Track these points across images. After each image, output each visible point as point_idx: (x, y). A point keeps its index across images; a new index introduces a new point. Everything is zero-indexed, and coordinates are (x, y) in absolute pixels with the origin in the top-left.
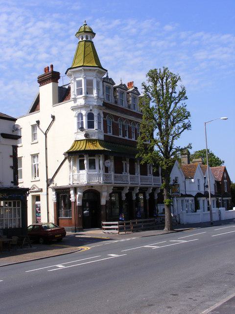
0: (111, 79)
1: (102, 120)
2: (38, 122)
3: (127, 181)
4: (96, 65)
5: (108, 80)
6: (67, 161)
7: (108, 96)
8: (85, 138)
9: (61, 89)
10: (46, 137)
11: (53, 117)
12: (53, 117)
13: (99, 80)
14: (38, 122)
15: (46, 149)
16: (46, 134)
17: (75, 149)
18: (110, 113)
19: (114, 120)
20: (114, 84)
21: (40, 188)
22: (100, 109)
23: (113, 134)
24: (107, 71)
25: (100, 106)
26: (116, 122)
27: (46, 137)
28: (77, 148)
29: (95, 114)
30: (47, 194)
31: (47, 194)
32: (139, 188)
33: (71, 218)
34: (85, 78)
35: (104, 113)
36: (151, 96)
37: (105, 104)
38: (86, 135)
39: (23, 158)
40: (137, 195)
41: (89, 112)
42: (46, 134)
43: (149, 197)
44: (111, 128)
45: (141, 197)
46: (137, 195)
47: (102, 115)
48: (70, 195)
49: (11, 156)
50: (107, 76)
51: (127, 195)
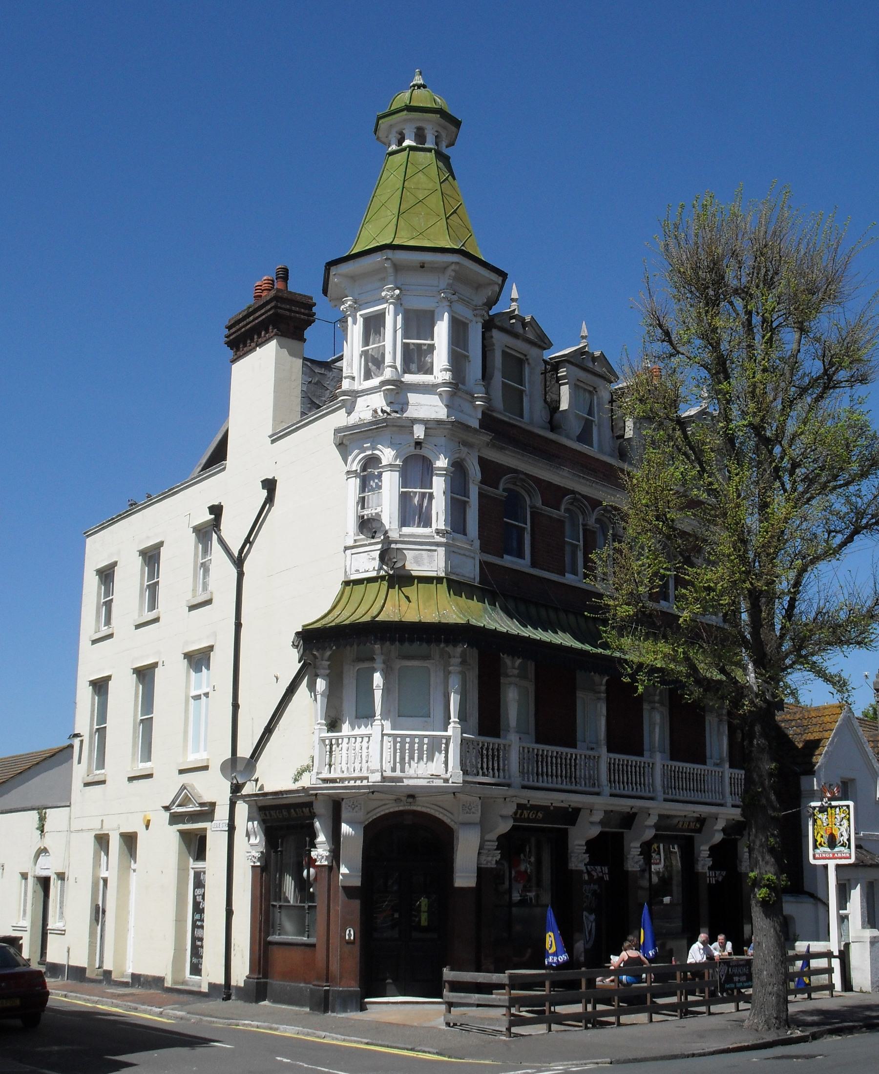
1: (474, 491)
2: (216, 511)
3: (594, 781)
6: (221, 980)
7: (514, 398)
11: (270, 485)
12: (270, 485)
13: (466, 313)
14: (216, 511)
15: (238, 626)
16: (239, 562)
17: (345, 616)
19: (539, 503)
20: (543, 343)
21: (207, 799)
22: (465, 444)
23: (534, 565)
25: (467, 428)
26: (554, 513)
27: (241, 575)
28: (346, 614)
33: (312, 940)
34: (399, 302)
35: (483, 463)
37: (489, 421)
39: (157, 671)
41: (412, 450)
42: (239, 562)
46: (647, 850)
47: (475, 472)
49: (37, 829)
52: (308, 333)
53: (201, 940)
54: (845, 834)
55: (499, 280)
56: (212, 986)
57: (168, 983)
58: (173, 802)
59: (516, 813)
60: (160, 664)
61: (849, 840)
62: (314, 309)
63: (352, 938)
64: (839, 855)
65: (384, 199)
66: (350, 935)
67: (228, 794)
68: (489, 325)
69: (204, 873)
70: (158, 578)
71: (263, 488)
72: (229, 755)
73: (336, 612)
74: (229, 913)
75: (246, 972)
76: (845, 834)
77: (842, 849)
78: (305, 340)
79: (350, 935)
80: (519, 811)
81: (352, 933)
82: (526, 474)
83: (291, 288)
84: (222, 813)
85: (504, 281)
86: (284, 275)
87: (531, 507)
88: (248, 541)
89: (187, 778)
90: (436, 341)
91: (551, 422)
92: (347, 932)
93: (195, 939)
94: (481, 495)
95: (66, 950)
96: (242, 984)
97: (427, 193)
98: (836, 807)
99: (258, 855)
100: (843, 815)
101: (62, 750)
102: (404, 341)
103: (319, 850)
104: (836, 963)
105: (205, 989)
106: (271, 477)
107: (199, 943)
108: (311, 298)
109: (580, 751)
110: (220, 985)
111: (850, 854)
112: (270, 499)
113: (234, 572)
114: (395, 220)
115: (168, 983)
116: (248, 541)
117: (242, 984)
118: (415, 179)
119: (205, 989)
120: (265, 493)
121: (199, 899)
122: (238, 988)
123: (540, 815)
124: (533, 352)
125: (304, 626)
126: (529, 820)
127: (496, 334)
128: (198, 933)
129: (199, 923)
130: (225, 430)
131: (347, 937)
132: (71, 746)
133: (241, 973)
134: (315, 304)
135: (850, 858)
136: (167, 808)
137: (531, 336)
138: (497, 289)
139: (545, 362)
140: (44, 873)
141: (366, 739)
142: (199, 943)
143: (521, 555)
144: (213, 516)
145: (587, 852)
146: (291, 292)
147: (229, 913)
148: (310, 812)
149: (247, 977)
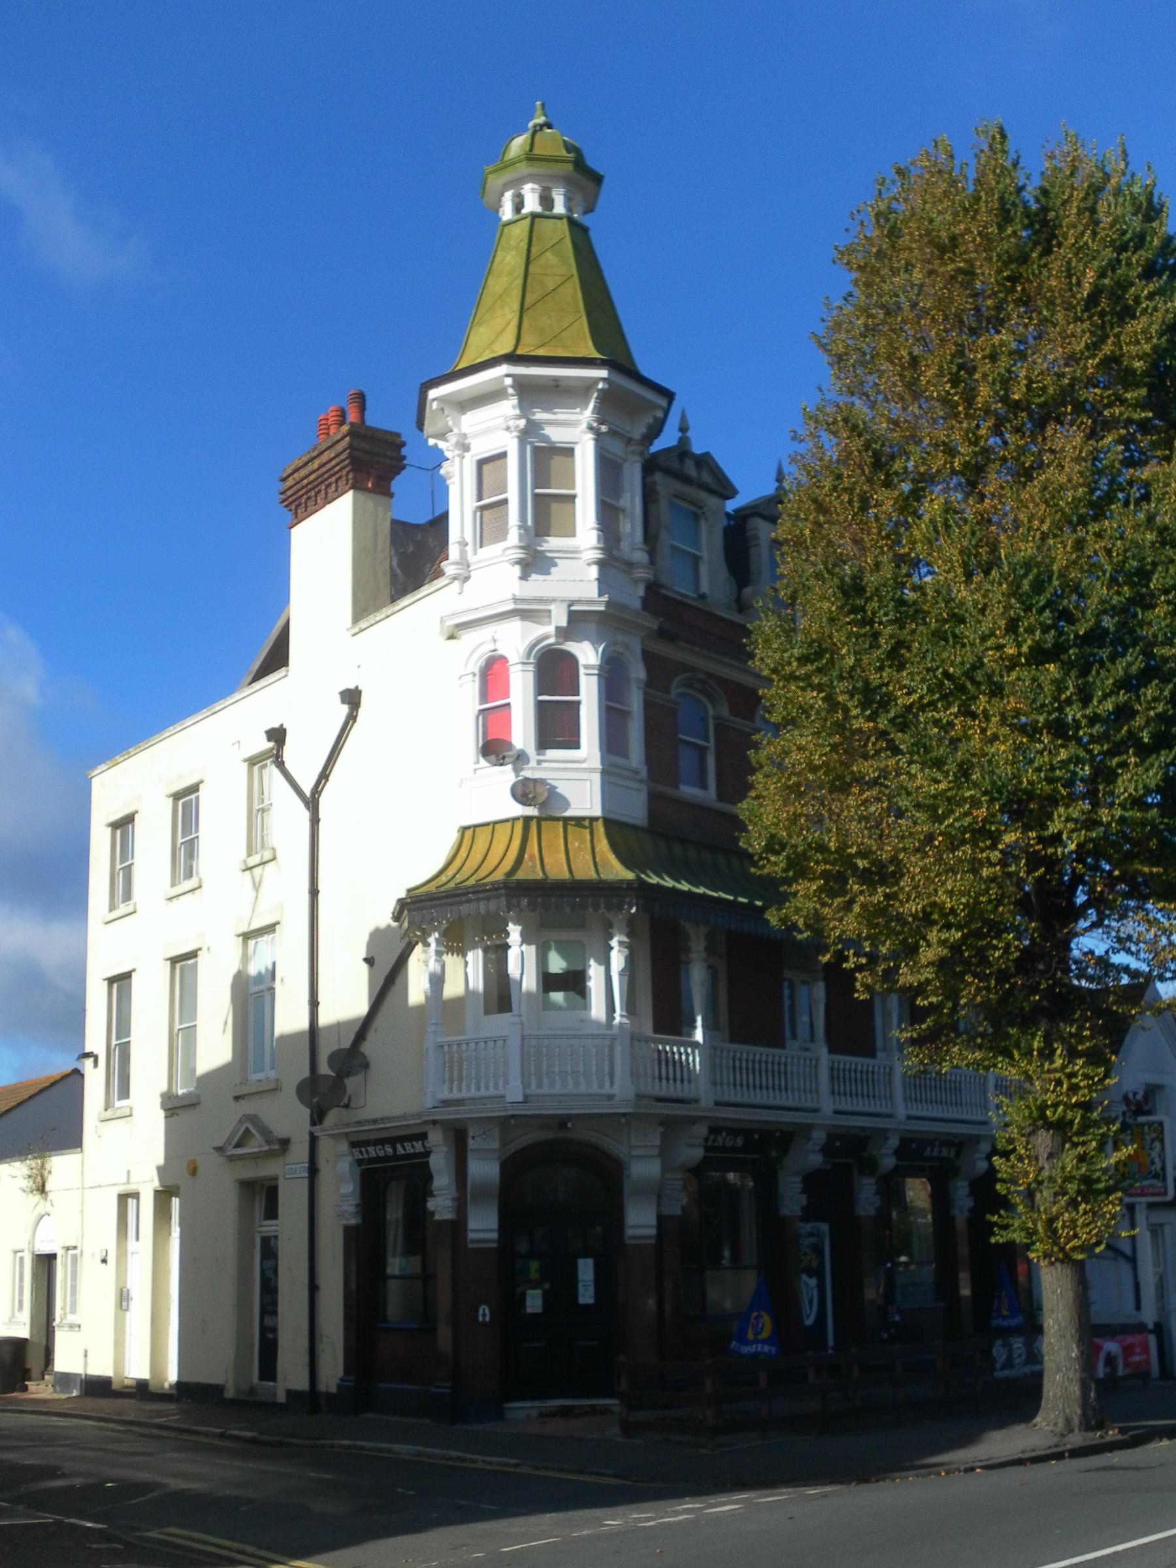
0: (705, 461)
2: (277, 736)
4: (595, 355)
5: (691, 469)
8: (617, 871)
9: (401, 531)
10: (315, 821)
11: (352, 698)
12: (352, 698)
14: (277, 736)
15: (314, 892)
16: (312, 803)
18: (700, 663)
19: (725, 712)
20: (726, 490)
23: (721, 797)
24: (669, 395)
27: (315, 821)
29: (587, 654)
30: (313, 1171)
31: (313, 1171)
32: (894, 1142)
36: (969, 685)
38: (523, 792)
40: (891, 1191)
42: (312, 803)
43: (804, 1200)
44: (711, 761)
45: (918, 1192)
47: (638, 672)
48: (429, 1178)
50: (684, 442)
51: (812, 1181)
52: (397, 484)
53: (274, 1330)
54: (1157, 1160)
55: (663, 402)
56: (290, 1393)
57: (230, 1393)
58: (229, 1140)
59: (706, 1139)
60: (205, 949)
61: (1163, 1169)
62: (404, 451)
63: (487, 1319)
64: (1151, 1190)
65: (499, 289)
66: (484, 1315)
67: (306, 1126)
68: (651, 466)
69: (276, 1237)
70: (197, 831)
71: (343, 702)
72: (306, 1073)
73: (443, 879)
74: (313, 1288)
75: (340, 1372)
76: (1157, 1160)
77: (1154, 1182)
78: (391, 495)
79: (484, 1315)
80: (712, 1137)
81: (487, 1311)
82: (707, 673)
83: (369, 422)
84: (299, 1152)
85: (670, 403)
86: (361, 400)
87: (715, 718)
88: (324, 776)
89: (248, 1107)
90: (578, 490)
91: (738, 600)
92: (481, 1311)
93: (264, 1330)
94: (648, 704)
95: (82, 1353)
96: (333, 1389)
97: (559, 280)
98: (1143, 1125)
99: (352, 1209)
100: (1154, 1135)
101: (65, 1077)
102: (538, 491)
103: (438, 1199)
104: (1152, 1340)
105: (281, 1398)
106: (352, 687)
107: (270, 1336)
108: (398, 435)
109: (792, 1047)
110: (304, 1392)
111: (1166, 1189)
112: (352, 718)
113: (306, 815)
114: (515, 322)
115: (230, 1393)
116: (324, 776)
117: (333, 1389)
118: (542, 261)
119: (281, 1398)
120: (345, 709)
121: (269, 1274)
122: (328, 1395)
123: (740, 1142)
124: (712, 501)
125: (409, 891)
126: (724, 1149)
127: (658, 477)
128: (268, 1321)
129: (269, 1308)
130: (280, 623)
131: (481, 1319)
132: (78, 1074)
133: (332, 1372)
134: (403, 444)
135: (1165, 1193)
136: (219, 1149)
137: (706, 478)
138: (660, 414)
139: (728, 515)
140: (45, 1248)
141: (500, 1043)
142: (270, 1336)
143: (704, 786)
144: (271, 744)
145: (803, 1191)
146: (370, 428)
147: (313, 1288)
148: (424, 1147)
149: (342, 1380)
